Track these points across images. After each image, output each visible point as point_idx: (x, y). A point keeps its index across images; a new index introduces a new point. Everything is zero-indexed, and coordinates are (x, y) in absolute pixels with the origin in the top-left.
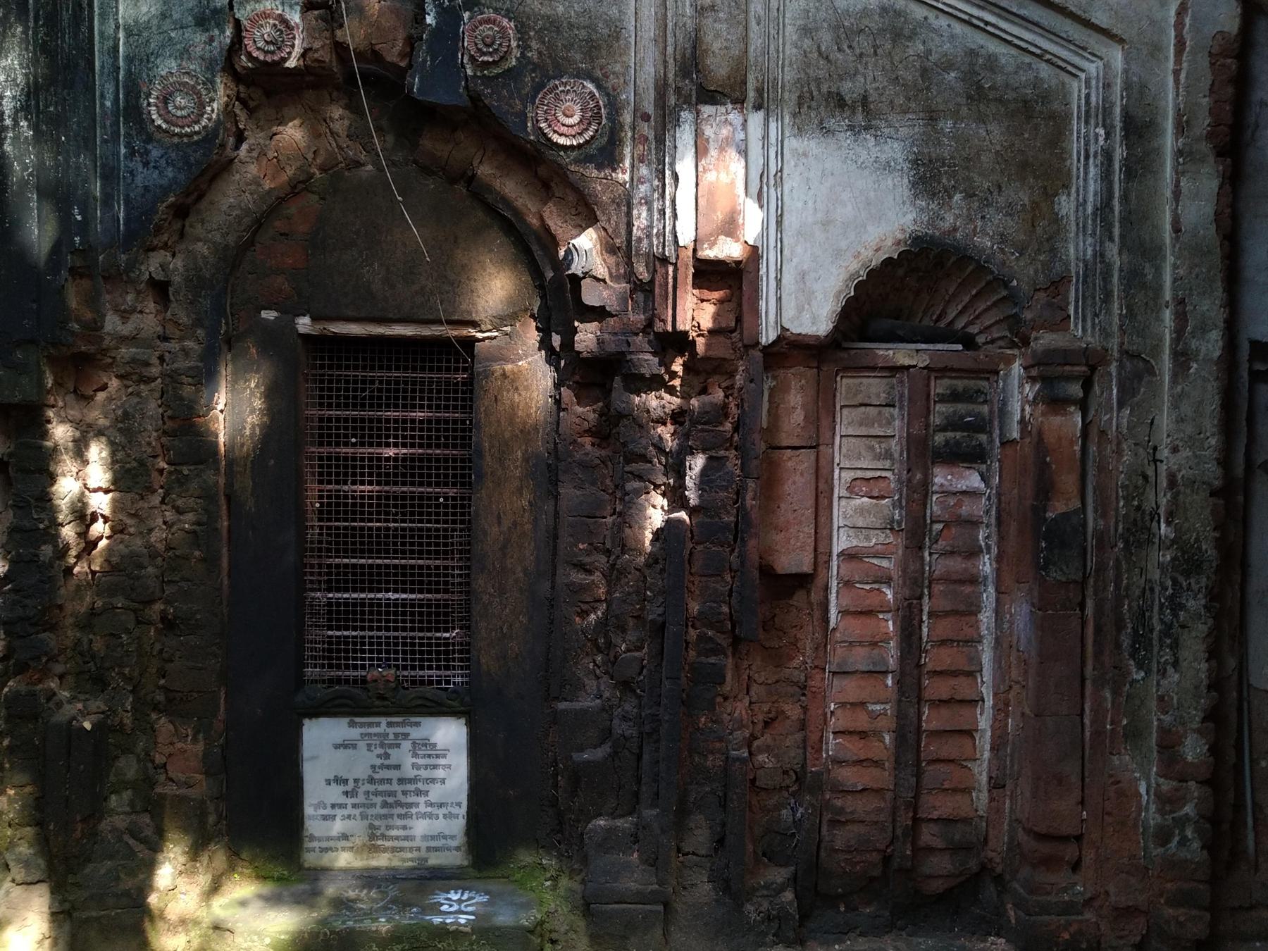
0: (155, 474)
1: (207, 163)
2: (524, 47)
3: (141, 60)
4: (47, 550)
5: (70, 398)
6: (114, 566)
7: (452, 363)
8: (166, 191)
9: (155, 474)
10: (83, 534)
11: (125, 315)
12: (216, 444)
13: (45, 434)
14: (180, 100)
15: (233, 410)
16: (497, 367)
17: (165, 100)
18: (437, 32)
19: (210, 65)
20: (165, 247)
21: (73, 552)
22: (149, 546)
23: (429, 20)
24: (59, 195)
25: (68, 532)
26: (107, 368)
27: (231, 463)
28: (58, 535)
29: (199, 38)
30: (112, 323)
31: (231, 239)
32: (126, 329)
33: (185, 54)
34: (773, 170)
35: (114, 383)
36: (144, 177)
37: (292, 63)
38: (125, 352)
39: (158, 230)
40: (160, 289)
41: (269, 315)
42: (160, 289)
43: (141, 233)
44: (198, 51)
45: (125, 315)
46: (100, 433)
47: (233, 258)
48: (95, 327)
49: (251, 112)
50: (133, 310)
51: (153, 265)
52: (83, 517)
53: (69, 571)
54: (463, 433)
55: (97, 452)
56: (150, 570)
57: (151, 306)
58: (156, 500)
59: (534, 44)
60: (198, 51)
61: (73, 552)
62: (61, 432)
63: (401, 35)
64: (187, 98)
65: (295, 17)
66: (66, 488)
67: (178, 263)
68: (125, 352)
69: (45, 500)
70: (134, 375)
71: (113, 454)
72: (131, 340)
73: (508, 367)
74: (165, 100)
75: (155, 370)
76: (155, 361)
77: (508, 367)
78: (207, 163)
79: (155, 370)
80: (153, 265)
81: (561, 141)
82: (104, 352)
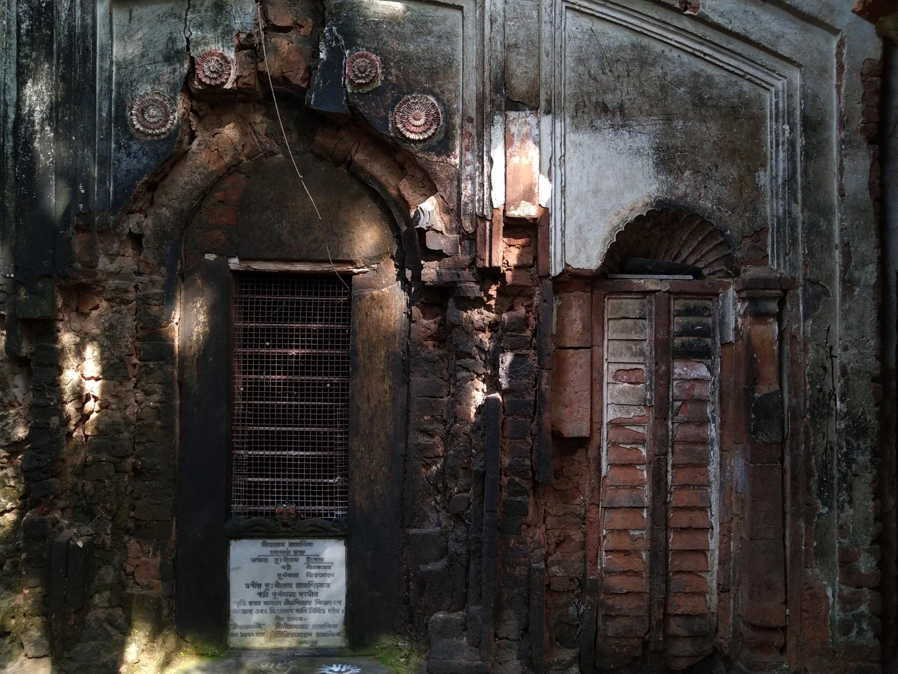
0: (130, 368)
1: (170, 153)
2: (387, 73)
3: (127, 85)
4: (55, 420)
5: (73, 315)
6: (105, 431)
7: (337, 290)
8: (141, 172)
9: (130, 368)
10: (80, 409)
11: (112, 257)
12: (172, 347)
13: (56, 340)
14: (152, 111)
15: (187, 323)
16: (367, 292)
17: (142, 112)
18: (327, 63)
19: (173, 88)
20: (140, 211)
21: (73, 422)
22: (125, 418)
23: (322, 56)
24: (71, 176)
25: (70, 408)
26: (99, 294)
27: (183, 359)
28: (63, 410)
29: (166, 69)
30: (103, 263)
31: (185, 206)
32: (112, 267)
33: (157, 80)
34: (558, 155)
35: (104, 304)
36: (127, 163)
37: (228, 86)
38: (112, 283)
39: (136, 199)
40: (136, 240)
41: (210, 257)
42: (136, 240)
43: (124, 202)
44: (165, 78)
45: (112, 257)
46: (93, 339)
47: (186, 219)
48: (91, 265)
49: (200, 119)
50: (118, 254)
51: (132, 223)
52: (81, 397)
53: (70, 434)
54: (343, 339)
55: (91, 352)
56: (126, 434)
57: (130, 251)
58: (131, 385)
59: (393, 71)
60: (165, 78)
61: (73, 422)
62: (67, 339)
63: (303, 66)
64: (157, 109)
65: (231, 55)
66: (70, 377)
67: (149, 222)
68: (112, 283)
69: (55, 385)
70: (118, 299)
71: (102, 353)
72: (116, 274)
73: (375, 292)
74: (142, 112)
75: (132, 296)
76: (132, 289)
77: (375, 292)
78: (170, 153)
79: (132, 296)
80: (132, 223)
81: (412, 136)
82: (97, 283)
